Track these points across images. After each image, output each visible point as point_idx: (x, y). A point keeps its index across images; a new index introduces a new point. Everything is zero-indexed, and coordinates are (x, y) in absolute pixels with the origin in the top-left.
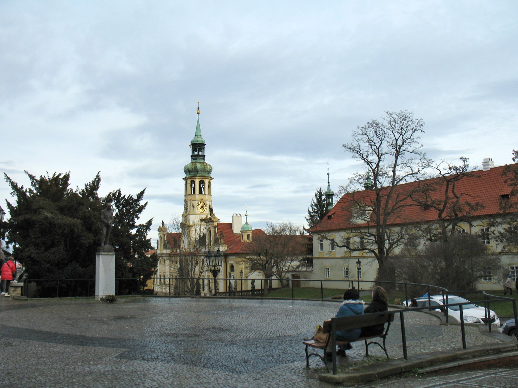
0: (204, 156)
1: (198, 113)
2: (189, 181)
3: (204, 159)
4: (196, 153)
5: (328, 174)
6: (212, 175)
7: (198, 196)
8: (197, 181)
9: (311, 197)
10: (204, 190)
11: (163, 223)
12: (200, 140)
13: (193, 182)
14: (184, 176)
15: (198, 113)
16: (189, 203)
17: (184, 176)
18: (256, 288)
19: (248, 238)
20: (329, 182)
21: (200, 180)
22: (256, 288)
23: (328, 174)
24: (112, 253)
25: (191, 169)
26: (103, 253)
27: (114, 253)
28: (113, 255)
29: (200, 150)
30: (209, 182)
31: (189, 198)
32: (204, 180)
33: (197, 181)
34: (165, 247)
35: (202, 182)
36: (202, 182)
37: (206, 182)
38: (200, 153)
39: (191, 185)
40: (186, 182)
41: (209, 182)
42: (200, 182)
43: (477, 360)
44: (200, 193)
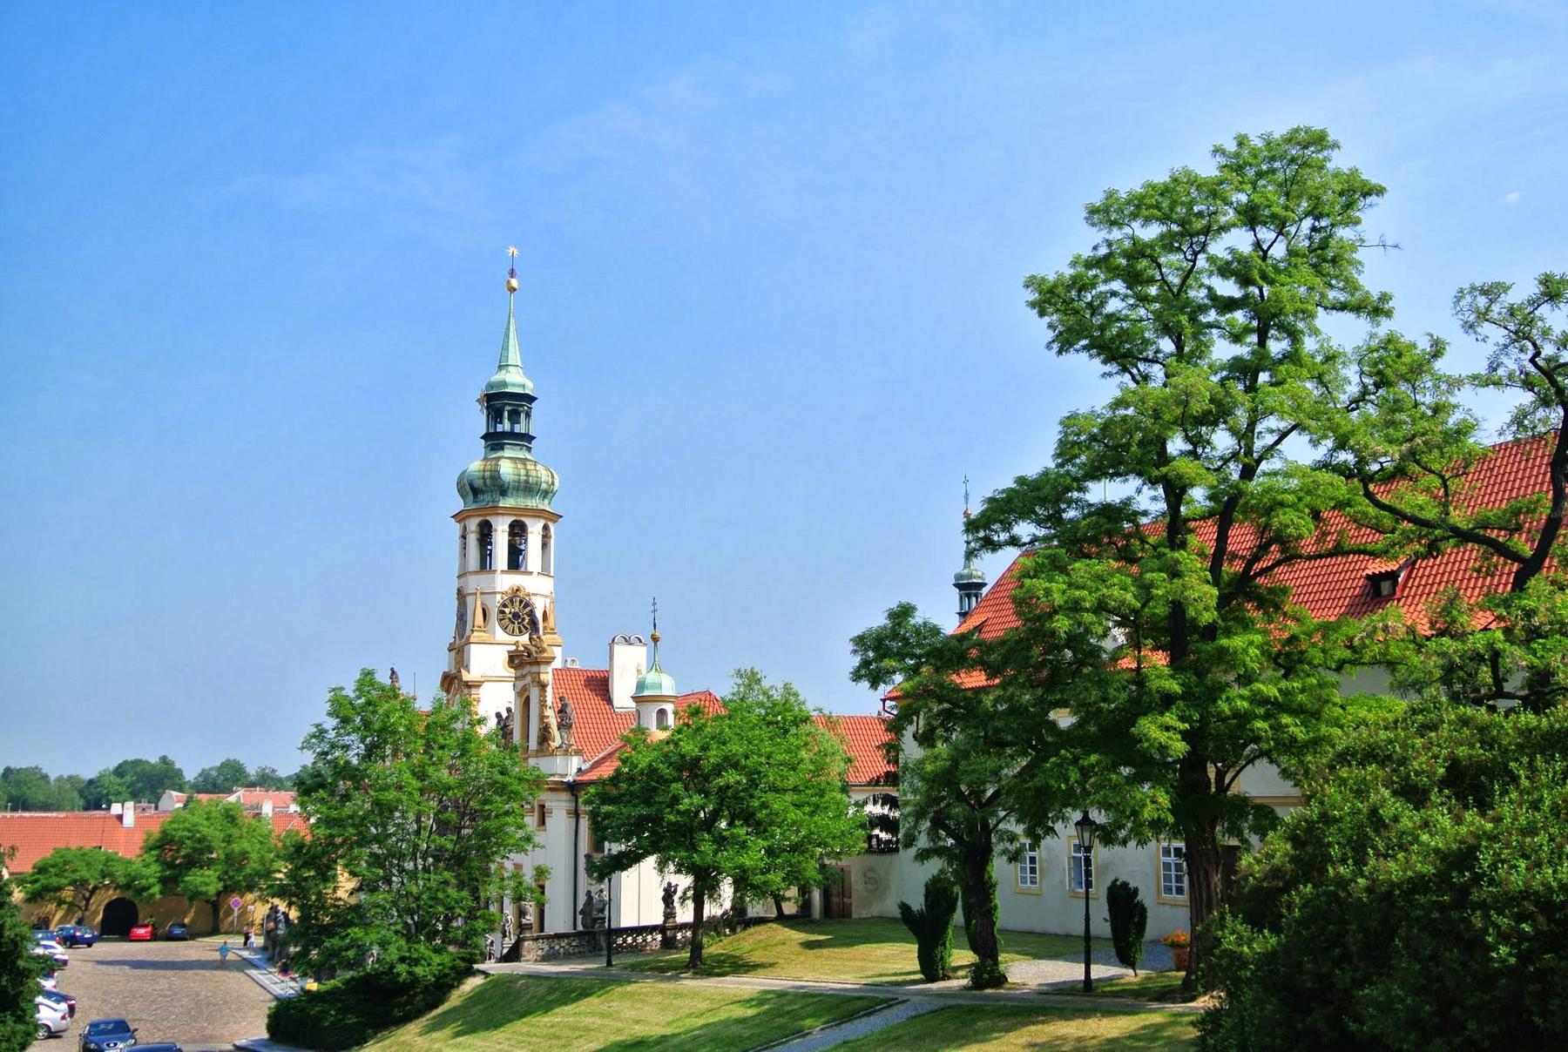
2: (473, 524)
13: (486, 533)
17: (458, 504)
21: (510, 519)
25: (478, 483)
30: (546, 528)
32: (526, 520)
35: (518, 530)
36: (518, 530)
38: (517, 429)
42: (512, 526)
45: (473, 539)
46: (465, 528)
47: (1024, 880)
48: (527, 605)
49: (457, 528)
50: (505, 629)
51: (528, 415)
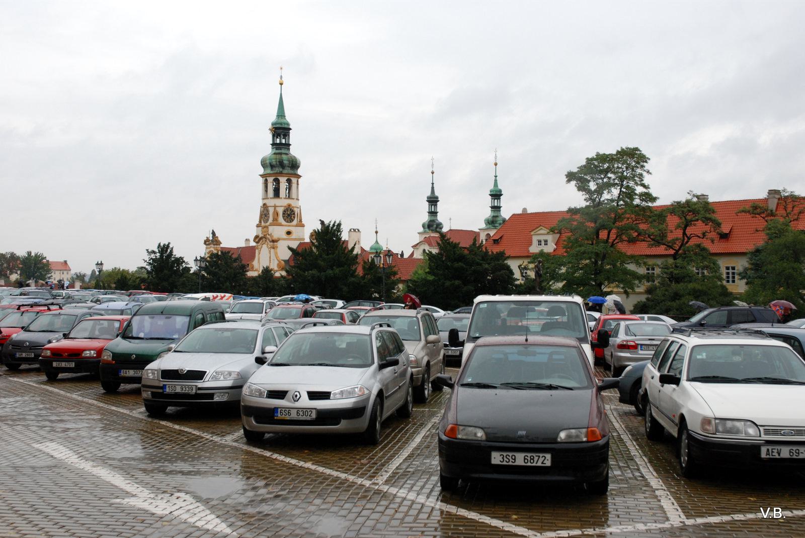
3: (289, 149)
4: (278, 141)
5: (433, 173)
6: (299, 172)
11: (213, 233)
15: (281, 84)
21: (286, 178)
23: (433, 173)
32: (292, 178)
33: (283, 180)
35: (289, 181)
37: (294, 180)
38: (283, 141)
40: (266, 180)
41: (298, 181)
46: (266, 180)
48: (293, 211)
50: (285, 220)
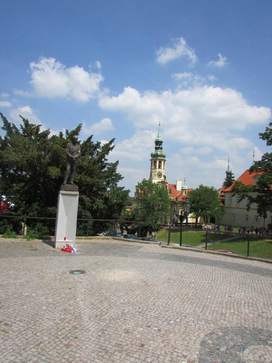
0: (162, 148)
1: (254, 156)
2: (153, 161)
4: (157, 147)
7: (158, 170)
8: (158, 162)
9: (151, 153)
10: (161, 166)
12: (160, 139)
13: (155, 162)
14: (151, 158)
16: (153, 173)
18: (188, 222)
19: (185, 193)
20: (229, 166)
22: (188, 222)
24: (75, 193)
26: (64, 192)
27: (78, 193)
28: (76, 195)
29: (160, 145)
31: (153, 171)
33: (158, 162)
34: (58, 178)
36: (160, 162)
38: (160, 147)
39: (154, 164)
43: (108, 220)
44: (159, 168)
45: (153, 164)
47: (246, 220)
48: (161, 174)
49: (150, 162)
51: (162, 144)
